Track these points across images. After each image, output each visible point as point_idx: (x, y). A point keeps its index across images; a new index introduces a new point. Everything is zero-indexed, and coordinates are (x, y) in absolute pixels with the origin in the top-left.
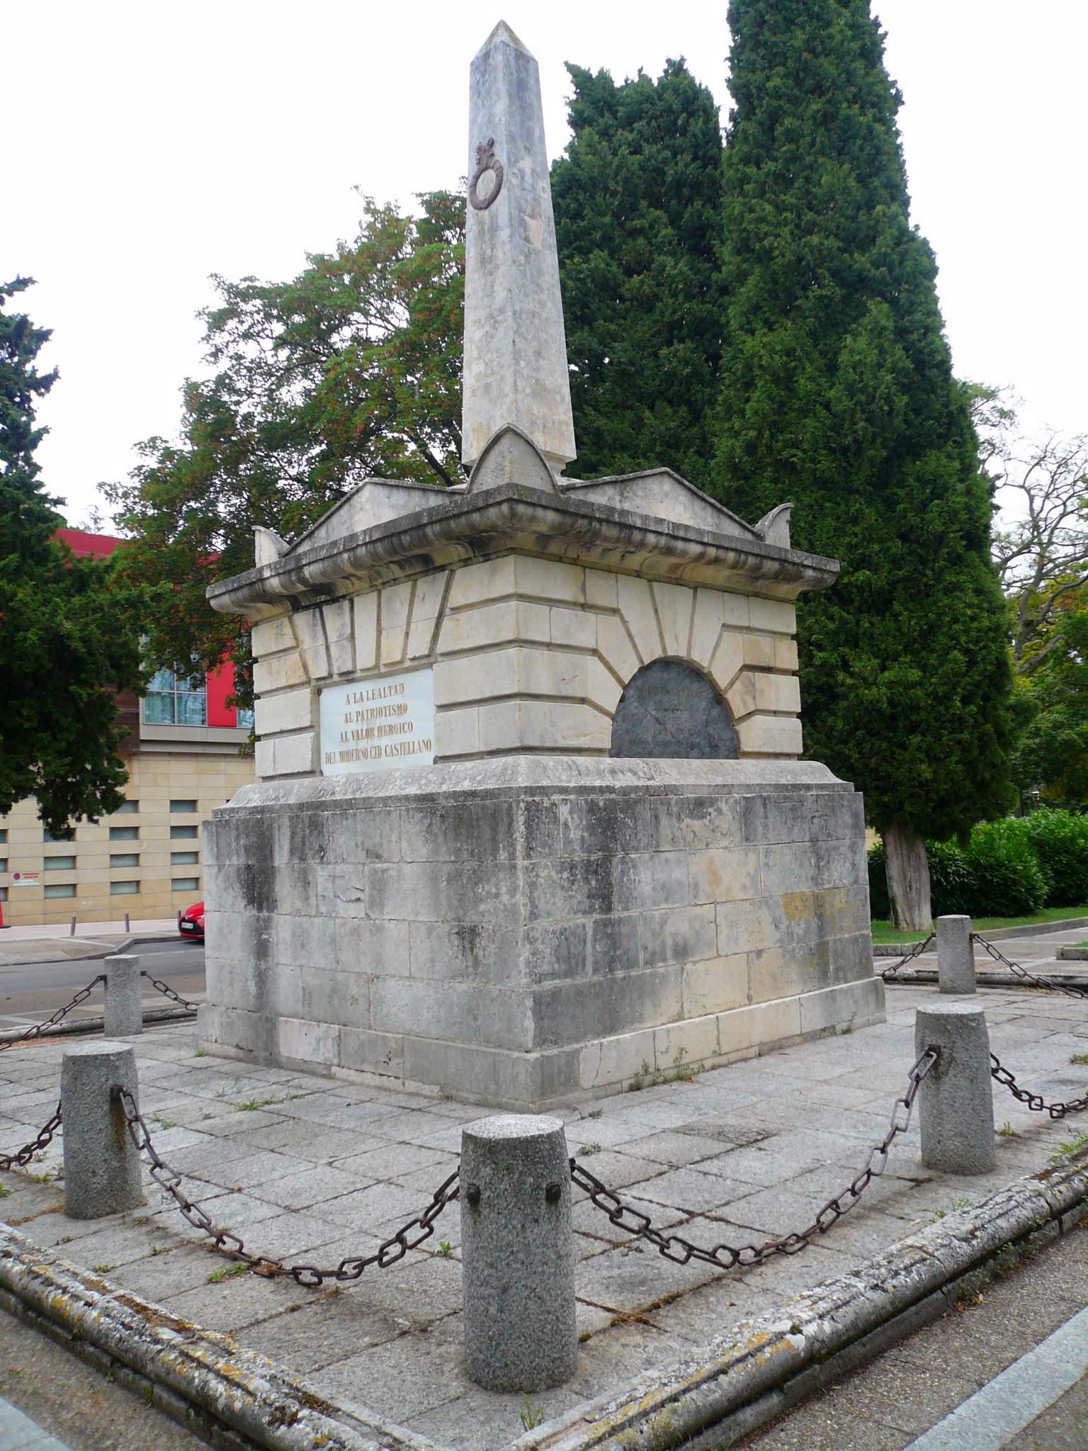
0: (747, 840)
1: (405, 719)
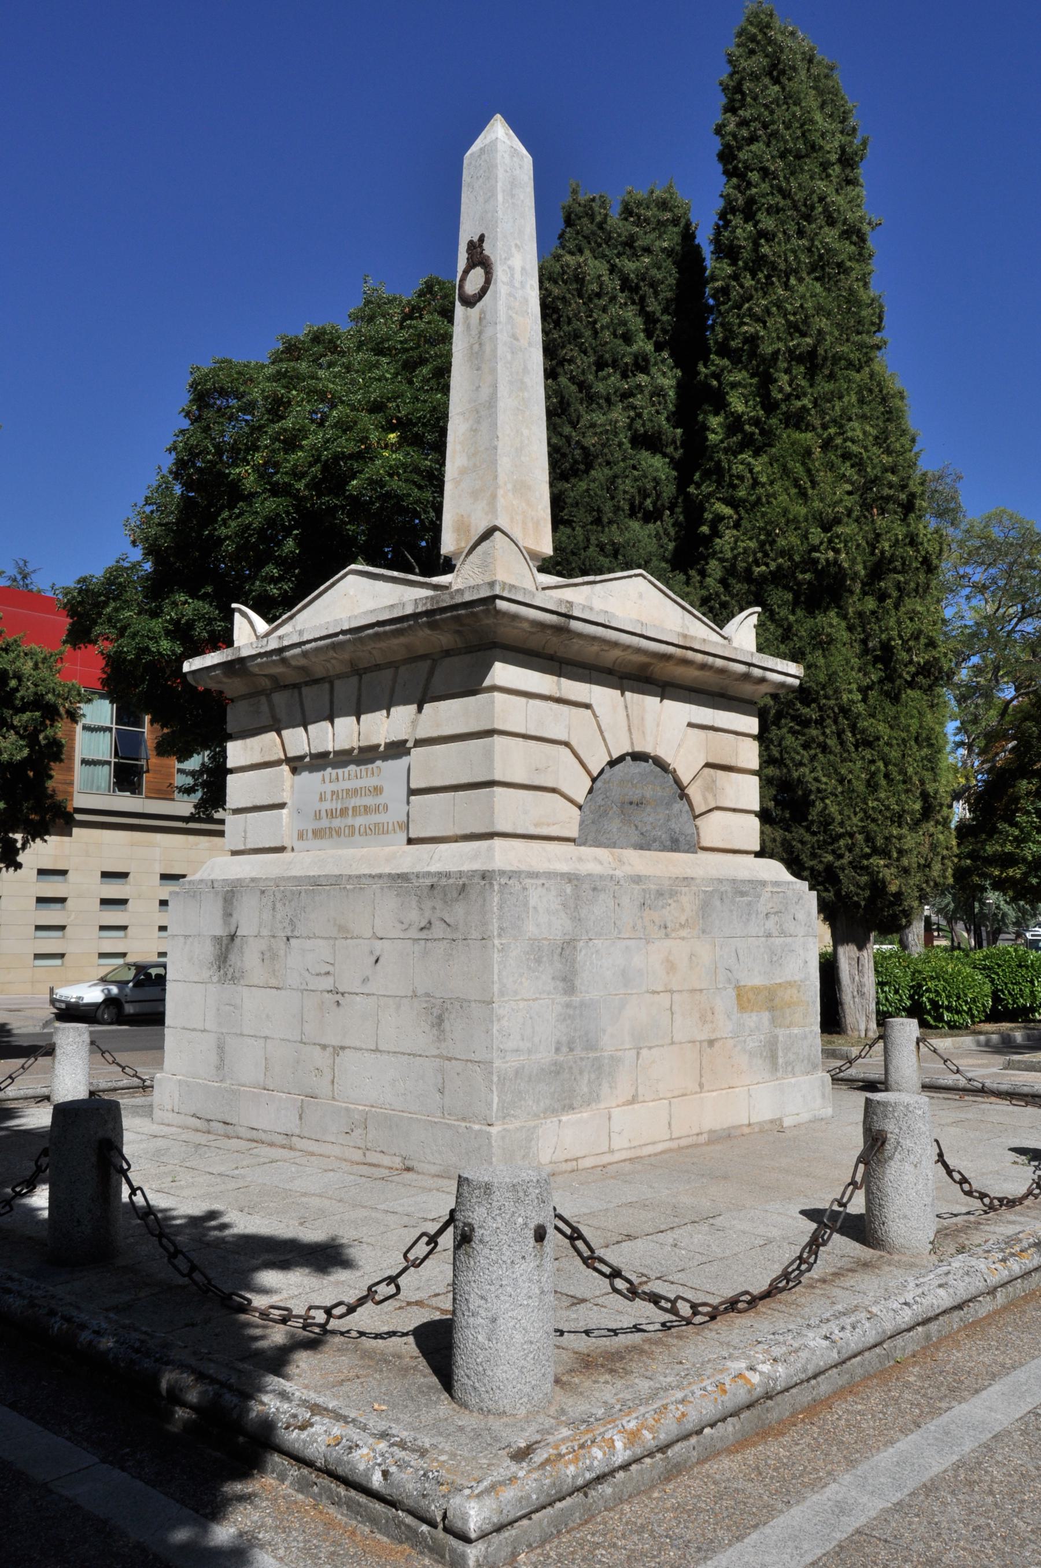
1: (380, 800)
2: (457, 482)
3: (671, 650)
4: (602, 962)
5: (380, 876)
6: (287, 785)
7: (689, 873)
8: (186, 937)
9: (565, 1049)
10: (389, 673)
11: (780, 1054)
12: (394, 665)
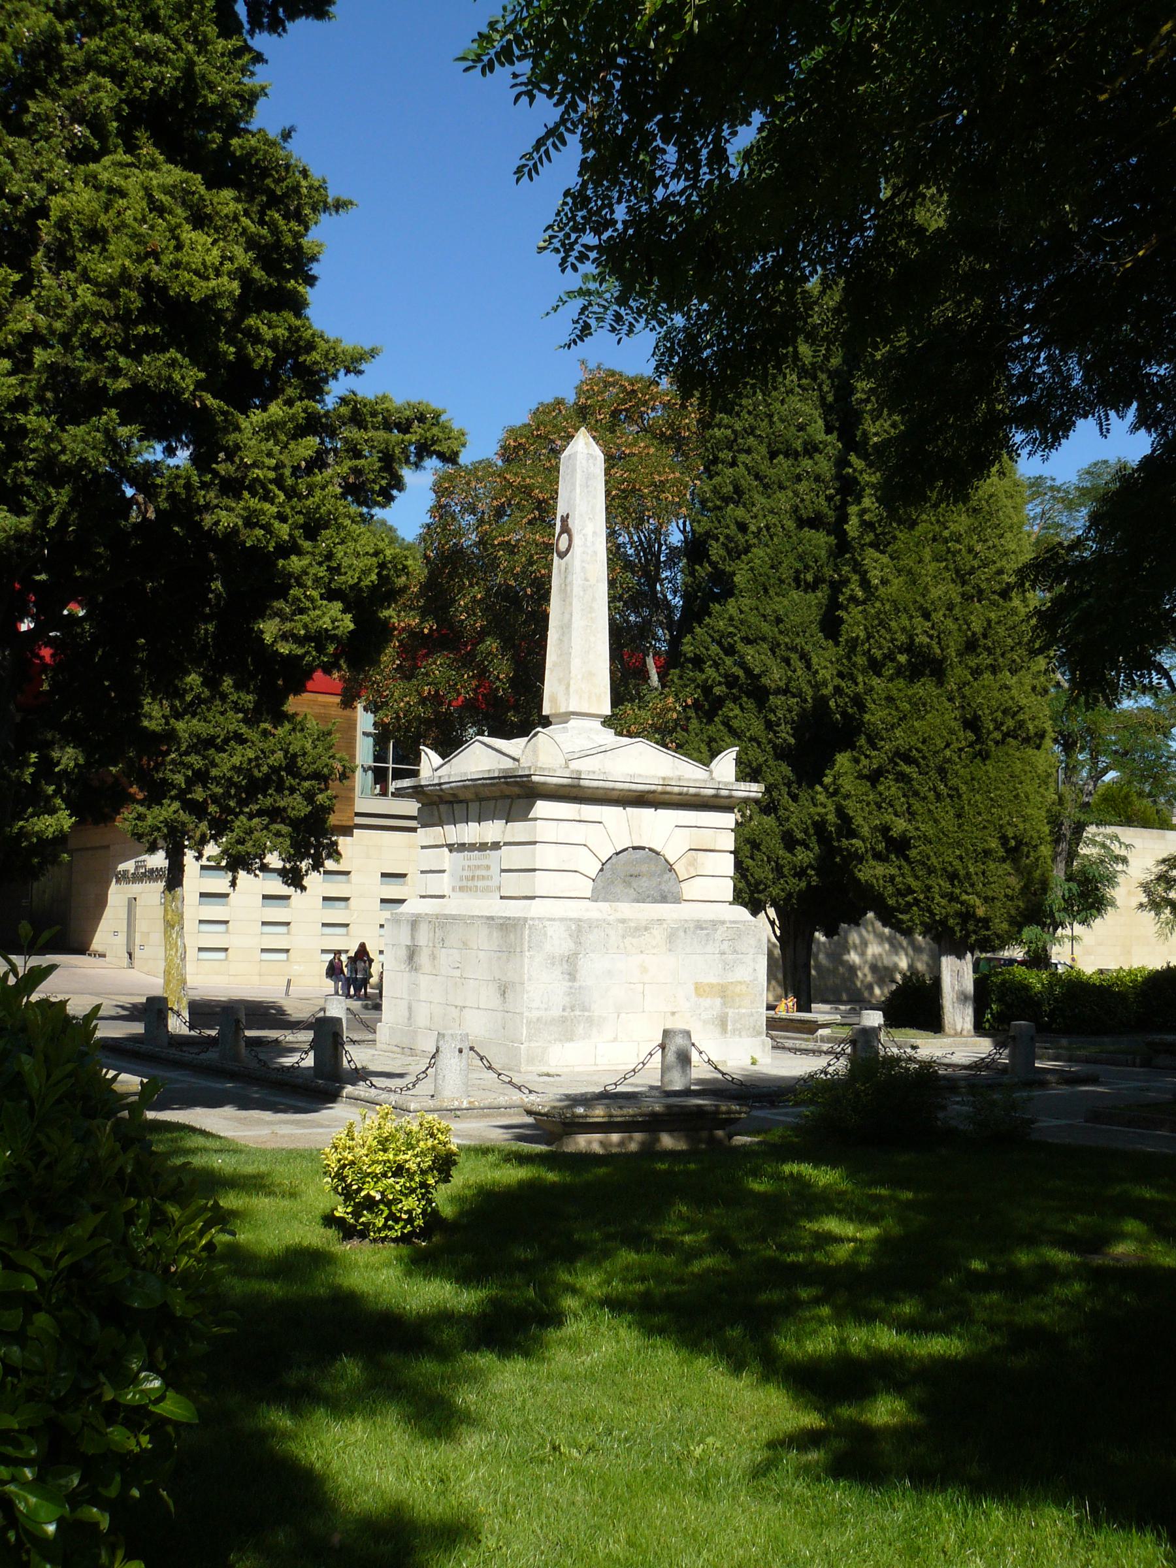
1: (489, 873)
2: (552, 671)
4: (592, 966)
6: (447, 859)
12: (495, 799)
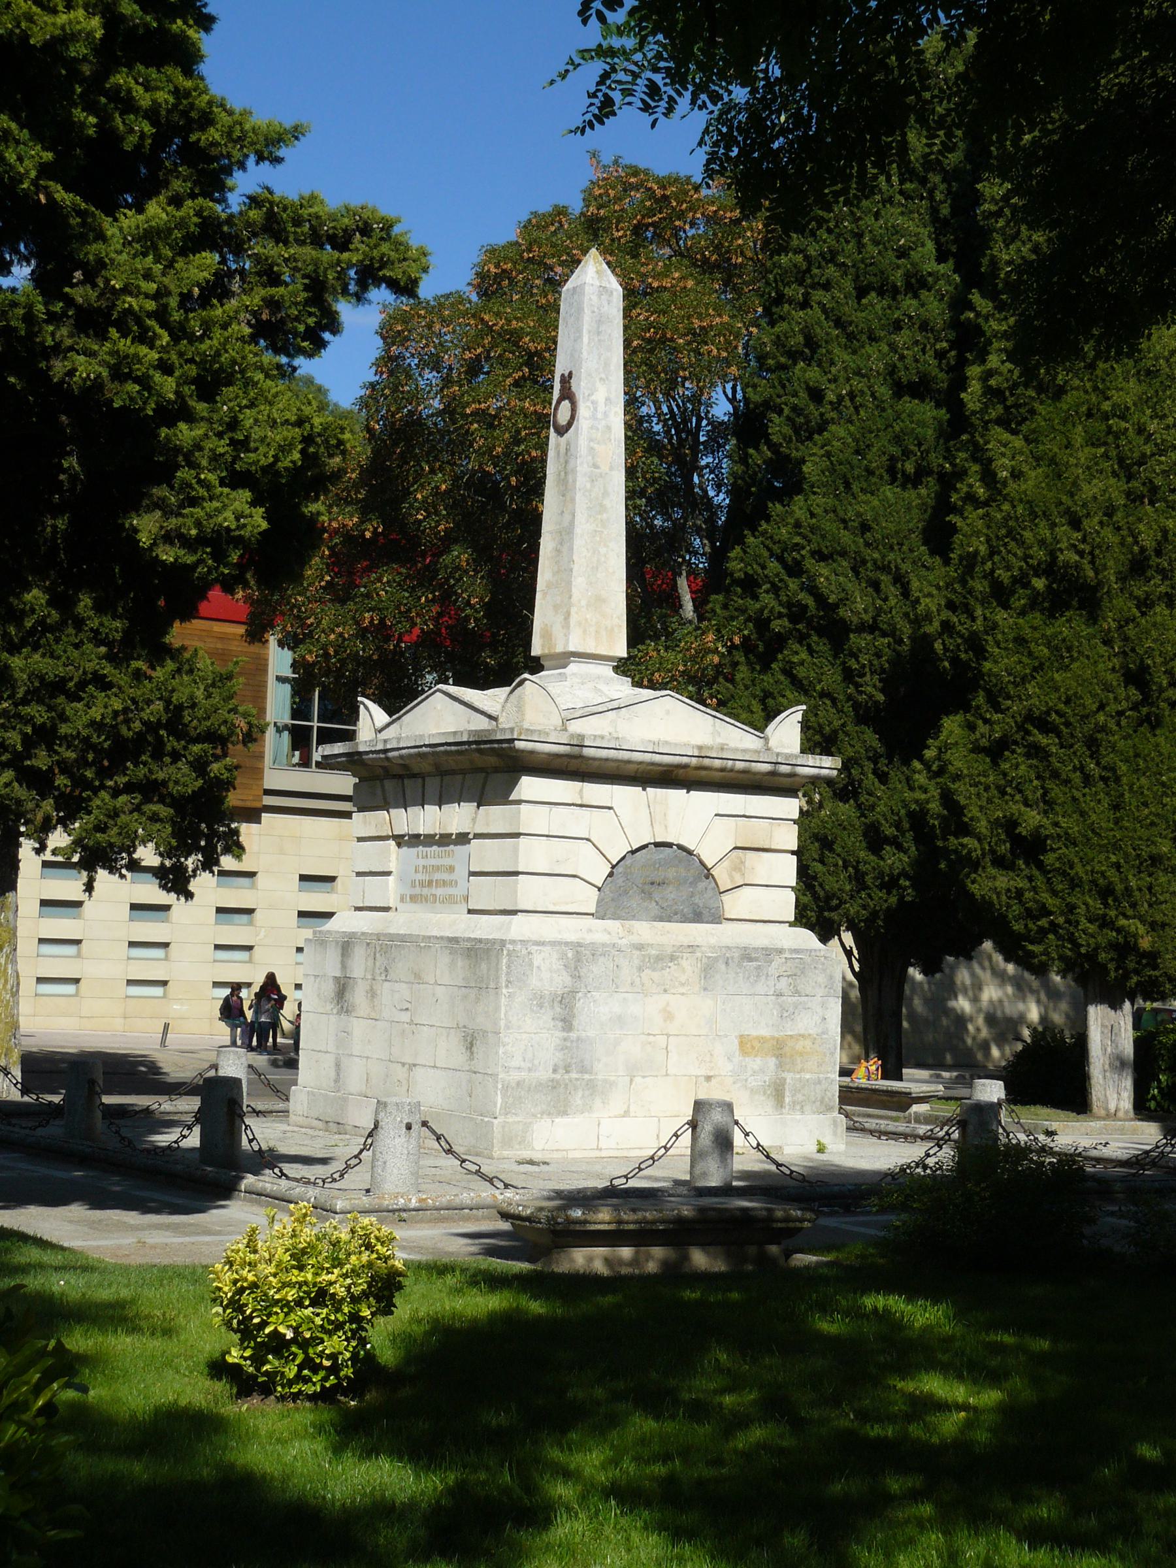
0: (705, 989)
1: (453, 877)
2: (545, 594)
3: (685, 760)
4: (597, 1010)
5: (442, 938)
6: (393, 857)
7: (699, 941)
8: (316, 976)
9: (561, 1071)
10: (460, 777)
11: (787, 1093)
12: (463, 772)
